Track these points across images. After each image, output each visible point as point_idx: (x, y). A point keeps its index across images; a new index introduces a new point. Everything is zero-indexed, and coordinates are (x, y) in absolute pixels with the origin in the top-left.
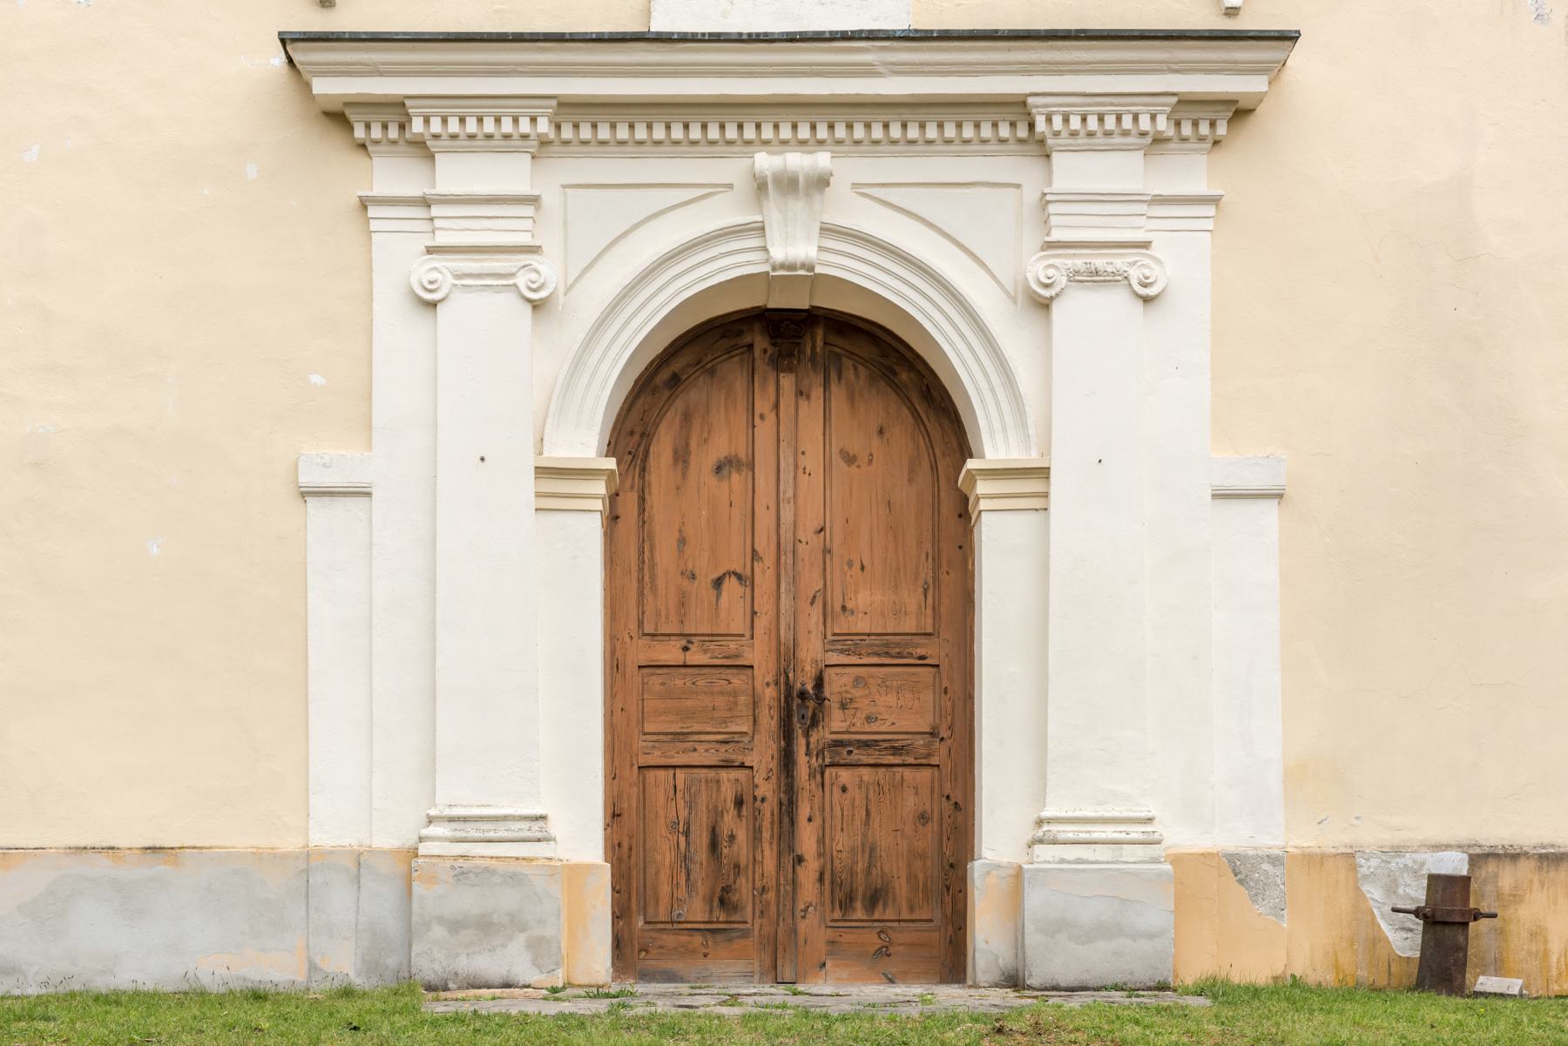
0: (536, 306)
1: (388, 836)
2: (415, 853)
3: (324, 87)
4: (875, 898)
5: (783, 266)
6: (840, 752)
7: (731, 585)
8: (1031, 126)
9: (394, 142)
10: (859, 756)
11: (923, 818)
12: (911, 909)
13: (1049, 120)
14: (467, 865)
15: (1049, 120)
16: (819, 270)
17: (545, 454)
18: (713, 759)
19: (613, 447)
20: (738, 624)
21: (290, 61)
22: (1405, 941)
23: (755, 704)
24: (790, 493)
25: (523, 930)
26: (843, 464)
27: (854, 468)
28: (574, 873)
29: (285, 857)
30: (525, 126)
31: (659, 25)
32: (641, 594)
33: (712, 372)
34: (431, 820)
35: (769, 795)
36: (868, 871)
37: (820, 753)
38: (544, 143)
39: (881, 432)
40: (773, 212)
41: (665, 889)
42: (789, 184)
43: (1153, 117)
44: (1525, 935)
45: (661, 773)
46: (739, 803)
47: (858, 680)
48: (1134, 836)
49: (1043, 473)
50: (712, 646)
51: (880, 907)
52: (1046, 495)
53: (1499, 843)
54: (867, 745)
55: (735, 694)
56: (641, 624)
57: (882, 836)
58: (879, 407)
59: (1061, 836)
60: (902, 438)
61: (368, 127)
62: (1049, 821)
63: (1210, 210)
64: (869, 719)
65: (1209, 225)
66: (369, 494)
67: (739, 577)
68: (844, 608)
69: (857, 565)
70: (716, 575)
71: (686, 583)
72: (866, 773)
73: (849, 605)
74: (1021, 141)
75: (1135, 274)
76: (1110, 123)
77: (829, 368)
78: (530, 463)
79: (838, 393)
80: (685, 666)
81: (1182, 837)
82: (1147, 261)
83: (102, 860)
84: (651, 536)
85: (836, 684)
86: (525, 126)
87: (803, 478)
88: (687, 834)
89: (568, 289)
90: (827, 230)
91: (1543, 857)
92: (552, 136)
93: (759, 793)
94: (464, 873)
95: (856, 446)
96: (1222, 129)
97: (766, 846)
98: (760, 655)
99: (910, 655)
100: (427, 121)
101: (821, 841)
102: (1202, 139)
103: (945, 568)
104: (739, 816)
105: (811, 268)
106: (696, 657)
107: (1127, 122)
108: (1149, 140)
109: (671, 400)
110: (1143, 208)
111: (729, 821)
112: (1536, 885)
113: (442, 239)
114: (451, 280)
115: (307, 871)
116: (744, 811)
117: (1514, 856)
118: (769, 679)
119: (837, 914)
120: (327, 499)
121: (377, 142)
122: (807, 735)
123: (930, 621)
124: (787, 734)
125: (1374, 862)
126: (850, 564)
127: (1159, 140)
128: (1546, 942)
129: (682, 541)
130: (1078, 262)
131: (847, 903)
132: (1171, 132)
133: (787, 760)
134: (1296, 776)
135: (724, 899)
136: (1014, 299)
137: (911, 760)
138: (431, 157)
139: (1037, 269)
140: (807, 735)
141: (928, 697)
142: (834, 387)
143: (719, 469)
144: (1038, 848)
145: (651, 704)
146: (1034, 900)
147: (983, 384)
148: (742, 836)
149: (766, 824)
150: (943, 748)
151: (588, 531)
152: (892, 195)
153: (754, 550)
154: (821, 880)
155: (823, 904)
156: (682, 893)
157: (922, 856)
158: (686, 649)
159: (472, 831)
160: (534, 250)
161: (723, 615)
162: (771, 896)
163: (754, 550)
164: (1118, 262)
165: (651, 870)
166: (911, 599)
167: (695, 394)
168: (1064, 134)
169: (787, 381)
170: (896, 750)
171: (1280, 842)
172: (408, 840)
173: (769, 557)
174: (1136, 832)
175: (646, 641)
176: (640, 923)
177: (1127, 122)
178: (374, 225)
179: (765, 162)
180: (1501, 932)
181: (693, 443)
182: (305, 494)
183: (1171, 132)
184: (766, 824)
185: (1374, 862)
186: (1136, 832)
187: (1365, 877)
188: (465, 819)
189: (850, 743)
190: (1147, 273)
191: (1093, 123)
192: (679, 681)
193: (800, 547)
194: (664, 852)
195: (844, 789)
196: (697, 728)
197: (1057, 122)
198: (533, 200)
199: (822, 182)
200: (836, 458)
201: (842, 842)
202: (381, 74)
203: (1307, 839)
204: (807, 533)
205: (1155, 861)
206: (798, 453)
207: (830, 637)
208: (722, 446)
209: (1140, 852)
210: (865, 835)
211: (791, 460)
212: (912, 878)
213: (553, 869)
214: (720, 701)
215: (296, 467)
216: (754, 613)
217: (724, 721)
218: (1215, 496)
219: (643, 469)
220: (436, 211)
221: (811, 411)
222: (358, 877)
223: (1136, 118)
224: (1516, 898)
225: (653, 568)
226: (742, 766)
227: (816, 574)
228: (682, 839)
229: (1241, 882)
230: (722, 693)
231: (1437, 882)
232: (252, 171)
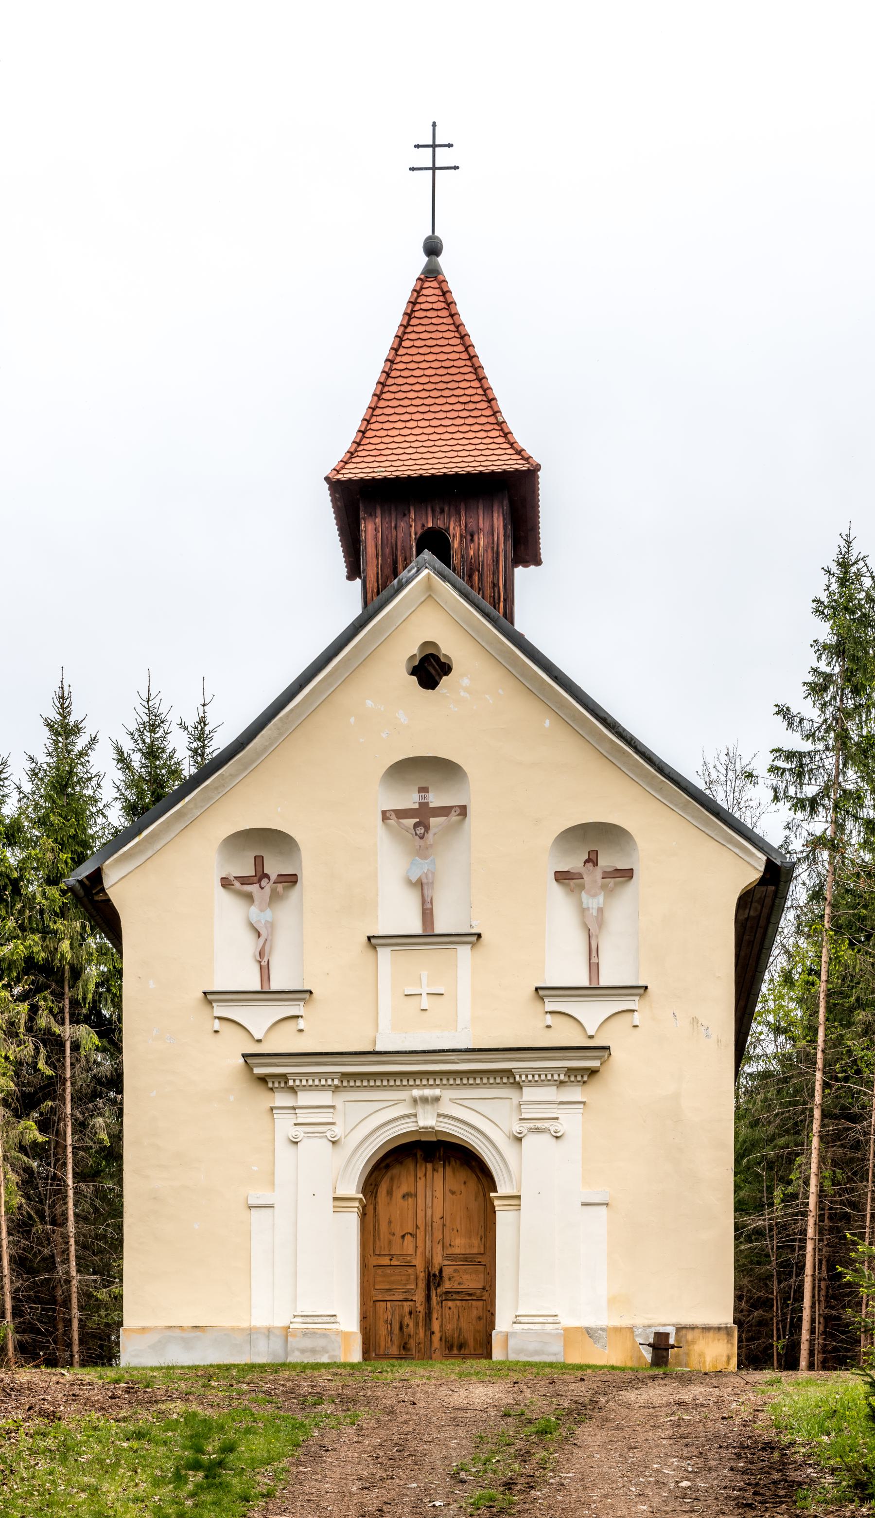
0: (334, 1143)
1: (281, 1321)
2: (289, 1328)
3: (257, 1071)
4: (461, 1346)
5: (423, 1128)
6: (448, 1295)
7: (408, 1238)
8: (515, 1078)
9: (283, 1088)
10: (455, 1296)
11: (479, 1318)
12: (475, 1350)
13: (520, 1076)
14: (307, 1331)
15: (520, 1076)
16: (437, 1128)
17: (337, 1193)
18: (401, 1298)
19: (364, 1191)
20: (411, 1251)
21: (246, 1061)
22: (647, 1355)
23: (417, 1278)
24: (430, 1205)
25: (327, 1353)
26: (450, 1194)
27: (454, 1196)
28: (347, 1335)
29: (243, 1329)
30: (329, 1082)
31: (378, 1049)
32: (374, 1241)
33: (401, 1163)
34: (295, 1316)
35: (422, 1310)
36: (459, 1337)
37: (441, 1296)
38: (337, 1087)
39: (465, 1183)
40: (420, 1110)
41: (383, 1344)
42: (425, 1100)
43: (559, 1075)
44: (697, 1355)
45: (382, 1303)
46: (410, 1313)
47: (455, 1270)
48: (549, 1321)
49: (518, 1197)
50: (401, 1259)
51: (463, 1349)
52: (519, 1205)
53: (688, 1324)
54: (458, 1293)
55: (409, 1275)
56: (374, 1251)
57: (464, 1325)
58: (464, 1174)
59: (523, 1321)
60: (473, 1184)
61: (273, 1083)
62: (519, 1316)
63: (582, 1106)
64: (459, 1284)
65: (581, 1111)
66: (273, 1207)
67: (411, 1234)
68: (450, 1245)
69: (455, 1230)
70: (402, 1234)
71: (391, 1237)
72: (458, 1303)
73: (452, 1244)
74: (511, 1083)
75: (552, 1129)
76: (543, 1077)
77: (446, 1160)
79: (449, 1170)
80: (391, 1266)
81: (568, 1321)
82: (557, 1124)
83: (178, 1331)
84: (378, 1220)
85: (447, 1272)
86: (329, 1082)
87: (435, 1200)
88: (391, 1324)
89: (346, 1136)
90: (439, 1115)
91: (703, 1328)
92: (340, 1085)
93: (418, 1310)
94: (306, 1334)
95: (455, 1188)
96: (585, 1078)
97: (420, 1328)
98: (418, 1262)
99: (475, 1261)
100: (294, 1081)
101: (441, 1326)
102: (579, 1082)
103: (488, 1231)
104: (411, 1318)
105: (433, 1128)
106: (394, 1262)
107: (549, 1077)
108: (558, 1083)
109: (386, 1173)
110: (556, 1106)
111: (407, 1320)
112: (701, 1338)
113: (300, 1121)
114: (303, 1134)
115: (250, 1334)
116: (412, 1316)
117: (693, 1328)
118: (422, 1270)
119: (447, 1352)
120: (258, 1209)
121: (277, 1088)
122: (436, 1289)
123: (483, 1249)
124: (428, 1288)
125: (640, 1330)
126: (453, 1230)
127: (562, 1082)
128: (704, 1358)
129: (390, 1222)
130: (531, 1125)
131: (450, 1348)
132: (566, 1079)
133: (428, 1298)
134: (613, 1301)
135: (405, 1347)
136: (509, 1138)
137: (475, 1298)
138: (296, 1092)
139: (516, 1128)
140: (436, 1289)
141: (482, 1276)
142: (447, 1168)
143: (404, 1197)
144: (515, 1325)
145: (378, 1279)
146: (512, 1342)
147: (497, 1167)
148: (411, 1325)
149: (421, 1321)
150: (487, 1294)
151: (351, 1221)
153: (417, 1225)
154: (441, 1340)
155: (442, 1348)
156: (389, 1344)
157: (479, 1332)
158: (391, 1260)
159: (309, 1320)
160: (333, 1124)
161: (405, 1247)
162: (422, 1346)
163: (417, 1225)
165: (377, 1337)
166: (476, 1242)
167: (395, 1171)
168: (526, 1081)
170: (470, 1295)
171: (606, 1324)
172: (285, 1323)
173: (422, 1228)
174: (550, 1320)
175: (376, 1257)
176: (374, 1355)
177: (549, 1077)
178: (275, 1116)
179: (416, 1093)
180: (688, 1354)
181: (394, 1188)
182: (250, 1207)
183: (566, 1079)
184: (421, 1321)
185: (640, 1330)
186: (550, 1320)
187: (637, 1335)
188: (307, 1316)
189: (452, 1292)
190: (557, 1128)
191: (536, 1077)
192: (388, 1271)
193: (434, 1224)
194: (383, 1331)
195: (450, 1308)
196: (395, 1287)
197: (524, 1077)
198: (333, 1107)
199: (437, 1099)
200: (448, 1192)
201: (449, 1327)
202: (278, 1066)
203: (616, 1322)
204: (437, 1218)
205: (557, 1329)
207: (445, 1255)
208: (404, 1189)
209: (551, 1326)
210: (457, 1324)
211: (431, 1193)
212: (475, 1339)
213: (338, 1332)
214: (403, 1278)
216: (416, 1247)
217: (405, 1285)
218: (582, 1205)
219: (376, 1197)
220: (297, 1111)
221: (439, 1176)
222: (269, 1336)
223: (552, 1075)
224: (694, 1342)
225: (379, 1232)
226: (412, 1300)
227: (440, 1232)
228: (389, 1326)
229: (590, 1337)
230: (404, 1275)
231: (658, 1335)
232: (232, 1098)
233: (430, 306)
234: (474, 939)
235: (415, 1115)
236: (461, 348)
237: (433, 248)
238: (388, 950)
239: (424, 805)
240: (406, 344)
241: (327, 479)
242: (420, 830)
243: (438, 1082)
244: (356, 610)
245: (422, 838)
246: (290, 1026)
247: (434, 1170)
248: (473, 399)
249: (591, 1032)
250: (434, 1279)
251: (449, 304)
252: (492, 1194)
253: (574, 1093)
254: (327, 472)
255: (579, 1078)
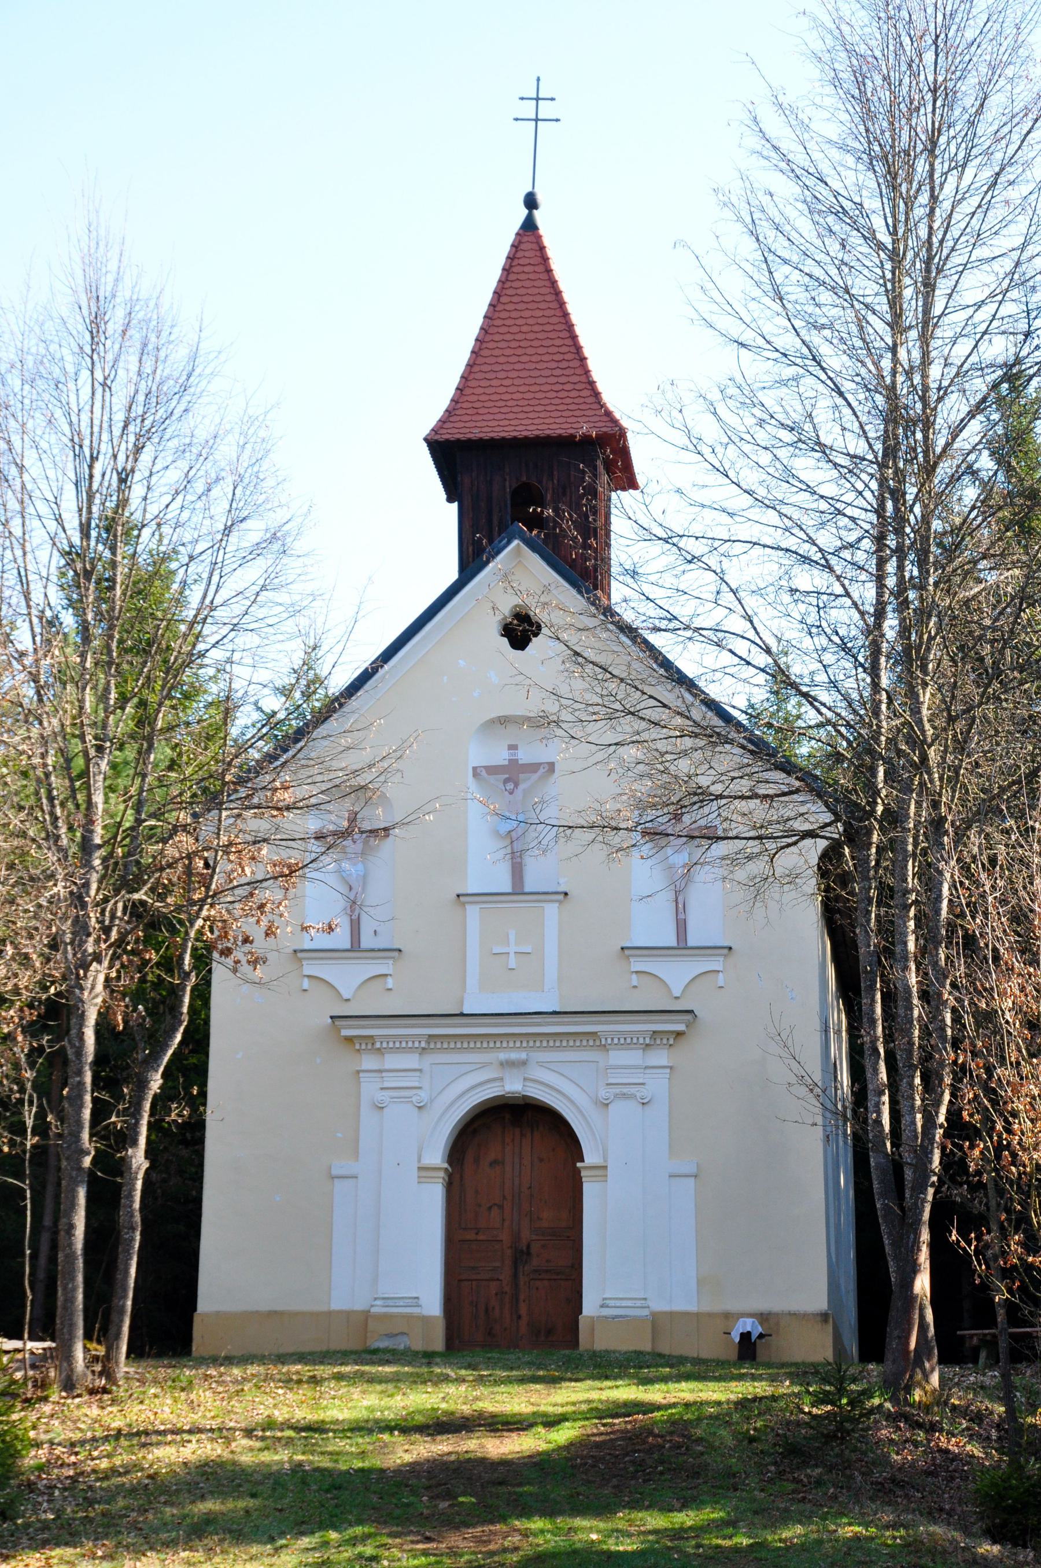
0: (419, 1108)
3: (345, 1032)
4: (549, 1332)
7: (495, 1211)
47: (543, 1246)
49: (605, 1167)
54: (547, 1271)
72: (546, 1283)
75: (638, 1095)
78: (416, 1165)
85: (535, 1248)
90: (525, 1079)
96: (671, 1042)
98: (505, 1237)
106: (481, 1237)
113: (386, 1085)
124: (515, 1263)
139: (603, 1093)
152: (553, 1066)
159: (390, 1302)
164: (633, 1090)
169: (517, 1131)
179: (503, 1056)
186: (639, 1303)
198: (420, 1070)
199: (524, 1063)
206: (521, 1158)
215: (330, 1168)
233: (527, 261)
234: (561, 897)
235: (501, 1079)
236: (555, 305)
237: (531, 202)
238: (477, 908)
239: (513, 762)
240: (503, 299)
241: (426, 440)
242: (510, 786)
243: (525, 1044)
244: (451, 574)
245: (511, 793)
246: (377, 984)
247: (522, 1135)
248: (566, 357)
249: (677, 993)
250: (521, 1255)
251: (545, 259)
252: (579, 1165)
253: (660, 1057)
254: (426, 430)
255: (665, 1041)
